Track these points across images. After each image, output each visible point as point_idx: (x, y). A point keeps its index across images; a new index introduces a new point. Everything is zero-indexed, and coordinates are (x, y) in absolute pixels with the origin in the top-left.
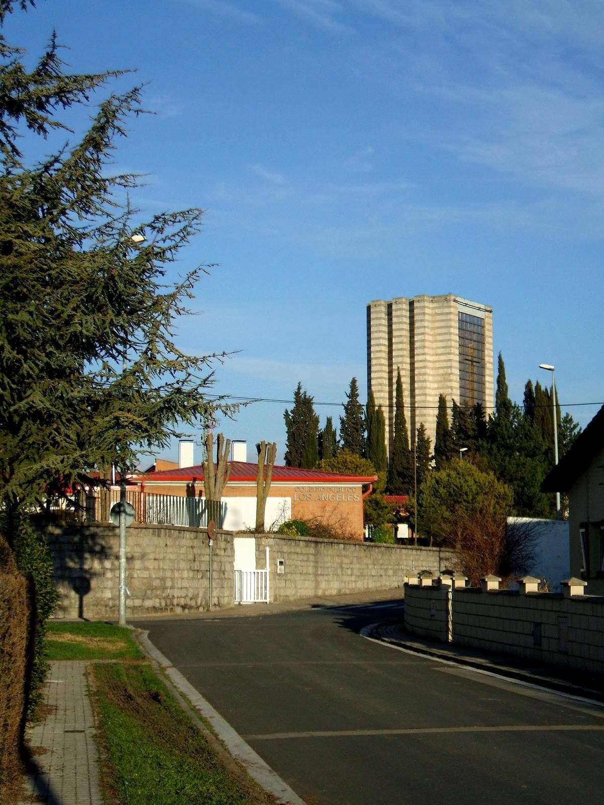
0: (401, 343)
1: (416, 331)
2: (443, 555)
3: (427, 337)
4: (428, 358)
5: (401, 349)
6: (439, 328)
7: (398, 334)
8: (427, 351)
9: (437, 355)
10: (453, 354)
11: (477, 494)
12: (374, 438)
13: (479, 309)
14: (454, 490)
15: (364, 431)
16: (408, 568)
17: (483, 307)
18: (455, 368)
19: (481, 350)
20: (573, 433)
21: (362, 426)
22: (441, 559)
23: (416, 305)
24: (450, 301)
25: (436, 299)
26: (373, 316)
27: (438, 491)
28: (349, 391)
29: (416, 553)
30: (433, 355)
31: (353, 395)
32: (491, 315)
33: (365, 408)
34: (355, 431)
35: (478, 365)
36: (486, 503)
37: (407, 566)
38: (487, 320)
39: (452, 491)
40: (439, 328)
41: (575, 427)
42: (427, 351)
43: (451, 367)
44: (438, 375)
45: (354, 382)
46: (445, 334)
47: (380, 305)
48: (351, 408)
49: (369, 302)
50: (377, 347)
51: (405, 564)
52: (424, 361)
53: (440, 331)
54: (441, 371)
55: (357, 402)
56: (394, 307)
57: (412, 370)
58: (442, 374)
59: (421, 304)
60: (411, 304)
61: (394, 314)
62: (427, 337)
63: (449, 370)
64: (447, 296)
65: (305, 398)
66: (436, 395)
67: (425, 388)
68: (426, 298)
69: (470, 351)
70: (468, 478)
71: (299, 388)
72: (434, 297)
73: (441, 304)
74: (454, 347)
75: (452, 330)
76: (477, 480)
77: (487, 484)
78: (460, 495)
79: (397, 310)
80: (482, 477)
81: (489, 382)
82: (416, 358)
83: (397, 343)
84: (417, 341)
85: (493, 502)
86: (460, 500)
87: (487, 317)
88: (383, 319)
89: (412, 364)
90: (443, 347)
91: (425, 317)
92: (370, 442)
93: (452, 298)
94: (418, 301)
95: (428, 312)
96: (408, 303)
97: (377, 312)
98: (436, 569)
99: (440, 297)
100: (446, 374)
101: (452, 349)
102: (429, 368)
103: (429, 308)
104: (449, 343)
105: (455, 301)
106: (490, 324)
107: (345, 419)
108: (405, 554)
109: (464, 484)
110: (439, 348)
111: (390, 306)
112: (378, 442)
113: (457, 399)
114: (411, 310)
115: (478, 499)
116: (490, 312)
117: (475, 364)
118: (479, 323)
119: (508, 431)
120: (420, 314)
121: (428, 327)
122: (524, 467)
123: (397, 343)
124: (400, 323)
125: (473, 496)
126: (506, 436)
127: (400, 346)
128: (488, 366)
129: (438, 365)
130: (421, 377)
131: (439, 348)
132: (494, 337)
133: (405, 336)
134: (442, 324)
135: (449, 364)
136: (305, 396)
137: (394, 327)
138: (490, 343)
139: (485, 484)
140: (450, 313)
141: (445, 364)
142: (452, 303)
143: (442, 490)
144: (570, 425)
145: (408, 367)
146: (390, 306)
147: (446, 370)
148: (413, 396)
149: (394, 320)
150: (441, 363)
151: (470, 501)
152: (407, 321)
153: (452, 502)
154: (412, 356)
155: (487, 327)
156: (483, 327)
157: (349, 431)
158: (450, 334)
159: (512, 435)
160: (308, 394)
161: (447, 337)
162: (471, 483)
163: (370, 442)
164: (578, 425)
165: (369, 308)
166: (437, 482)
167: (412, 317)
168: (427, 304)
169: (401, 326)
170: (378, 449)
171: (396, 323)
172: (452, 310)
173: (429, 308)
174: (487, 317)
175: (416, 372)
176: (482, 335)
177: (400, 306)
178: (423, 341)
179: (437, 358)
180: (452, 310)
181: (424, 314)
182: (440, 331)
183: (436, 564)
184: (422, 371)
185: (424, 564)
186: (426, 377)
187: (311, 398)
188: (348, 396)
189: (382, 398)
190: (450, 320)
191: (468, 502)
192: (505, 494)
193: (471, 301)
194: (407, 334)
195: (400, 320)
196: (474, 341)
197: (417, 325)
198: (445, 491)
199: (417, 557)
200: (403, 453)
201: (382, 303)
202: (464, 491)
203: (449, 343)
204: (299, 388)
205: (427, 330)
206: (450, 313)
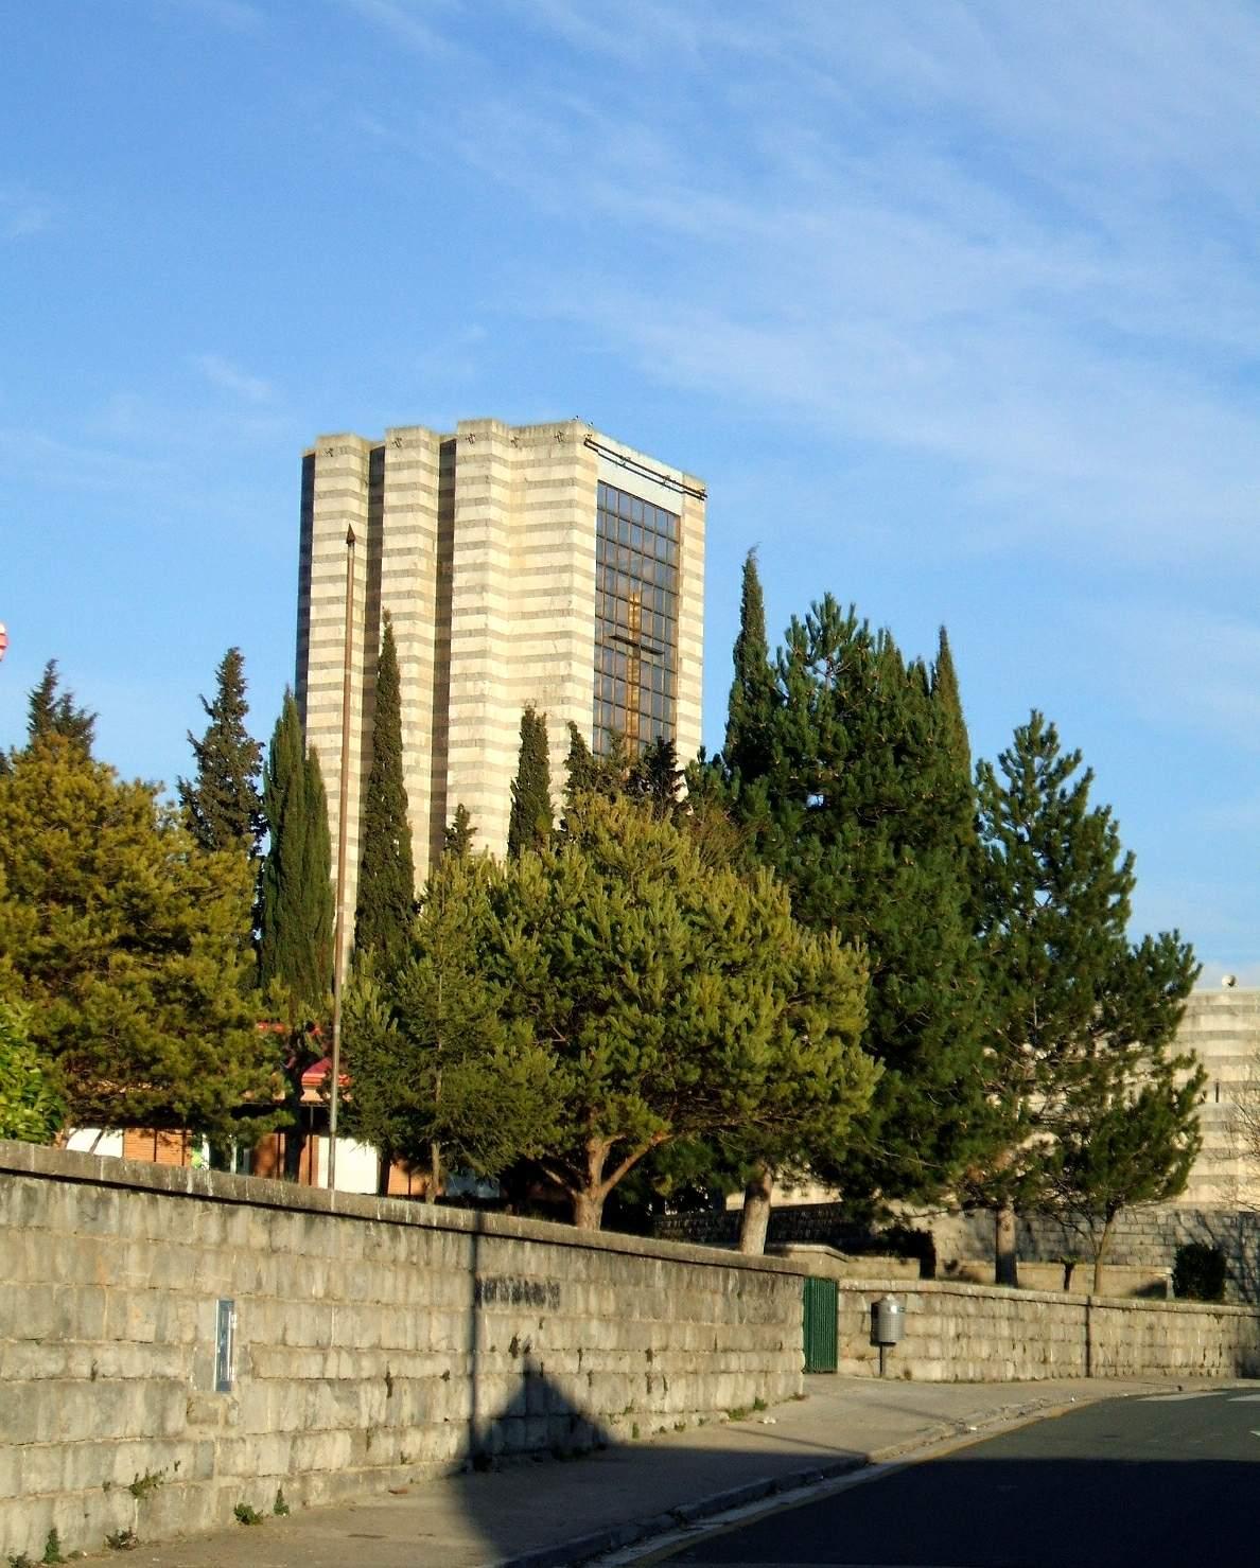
0: (407, 573)
1: (459, 536)
2: (499, 1260)
3: (494, 557)
4: (495, 623)
5: (410, 594)
6: (532, 528)
7: (401, 545)
8: (491, 600)
9: (526, 616)
10: (579, 614)
11: (689, 969)
12: (292, 855)
13: (665, 481)
14: (579, 943)
15: (261, 832)
16: (175, 1368)
17: (676, 475)
18: (582, 660)
19: (667, 615)
20: (1058, 790)
21: (254, 814)
22: (480, 1293)
23: (460, 450)
24: (572, 442)
25: (527, 436)
26: (320, 485)
27: (498, 949)
28: (213, 692)
29: (260, 1238)
30: (512, 616)
31: (229, 705)
32: (700, 506)
33: (265, 752)
34: (230, 829)
35: (655, 659)
36: (739, 1013)
37: (160, 1345)
38: (688, 522)
39: (569, 948)
40: (532, 528)
41: (1064, 769)
42: (491, 600)
43: (567, 656)
44: (526, 681)
45: (231, 675)
46: (552, 548)
47: (345, 450)
48: (220, 752)
49: (309, 444)
50: (330, 586)
51: (142, 1327)
52: (482, 632)
53: (537, 539)
54: (536, 670)
55: (241, 732)
56: (389, 458)
57: (442, 665)
58: (540, 680)
59: (480, 449)
60: (448, 450)
61: (390, 478)
62: (494, 557)
63: (562, 664)
64: (564, 425)
65: (67, 718)
66: (513, 705)
67: (481, 721)
68: (494, 429)
69: (625, 613)
70: (653, 891)
71: (49, 683)
72: (522, 430)
73: (542, 453)
74: (581, 593)
75: (577, 537)
76: (695, 901)
77: (742, 921)
78: (610, 967)
79: (398, 467)
80: (723, 892)
81: (688, 719)
82: (457, 623)
83: (396, 574)
84: (463, 569)
85: (769, 1012)
86: (605, 992)
87: (691, 512)
88: (355, 494)
89: (443, 644)
90: (546, 593)
91: (489, 490)
92: (279, 869)
93: (582, 432)
94: (470, 439)
95: (500, 477)
96: (436, 445)
97: (333, 473)
98: (442, 1364)
99: (544, 427)
100: (551, 679)
101: (574, 598)
102: (496, 657)
103: (504, 462)
104: (567, 515)
105: (588, 442)
106: (695, 535)
107: (196, 787)
108: (145, 1242)
109: (628, 917)
110: (531, 593)
111: (377, 457)
112: (306, 862)
113: (585, 718)
114: (447, 473)
115: (696, 990)
116: (700, 496)
117: (645, 656)
118: (664, 529)
119: (822, 730)
120: (473, 480)
121: (498, 525)
122: (889, 890)
123: (396, 574)
124: (410, 508)
125: (670, 977)
126: (812, 747)
127: (406, 584)
128: (689, 667)
129: (525, 649)
130: (470, 685)
131: (531, 593)
132: (707, 580)
133: (423, 553)
134: (546, 516)
135: (562, 645)
136: (67, 709)
137: (389, 521)
138: (694, 596)
139: (731, 921)
140: (573, 482)
141: (547, 647)
142: (580, 450)
143: (515, 942)
144: (1049, 757)
145: (429, 654)
146: (377, 457)
147: (549, 665)
148: (440, 748)
149: (390, 498)
150: (537, 643)
151: (658, 999)
152: (433, 503)
153: (568, 1003)
154: (443, 619)
155: (688, 542)
156: (677, 542)
157: (208, 830)
158: (570, 548)
159: (836, 744)
160: (77, 705)
161: (559, 559)
162: (665, 910)
163: (279, 869)
164: (1078, 758)
165: (309, 463)
166: (500, 906)
167: (447, 494)
168: (497, 449)
169: (410, 519)
170: (307, 893)
171: (394, 509)
172: (579, 472)
173: (504, 462)
174: (691, 512)
175: (455, 668)
176: (674, 567)
177: (409, 455)
178: (481, 567)
179: (522, 627)
180: (579, 472)
181: (487, 480)
182: (537, 539)
183: (445, 1332)
184: (475, 665)
185: (339, 1327)
186: (486, 687)
187: (87, 716)
188: (210, 712)
189: (335, 743)
190: (571, 504)
191: (647, 1006)
192: (829, 977)
193: (640, 452)
194: (430, 545)
195: (408, 498)
196: (646, 582)
197: (461, 515)
198: (534, 947)
199: (269, 1270)
200: (395, 909)
201: (353, 443)
202: (627, 947)
203: (567, 515)
204: (49, 683)
205: (495, 534)
206: (573, 482)
